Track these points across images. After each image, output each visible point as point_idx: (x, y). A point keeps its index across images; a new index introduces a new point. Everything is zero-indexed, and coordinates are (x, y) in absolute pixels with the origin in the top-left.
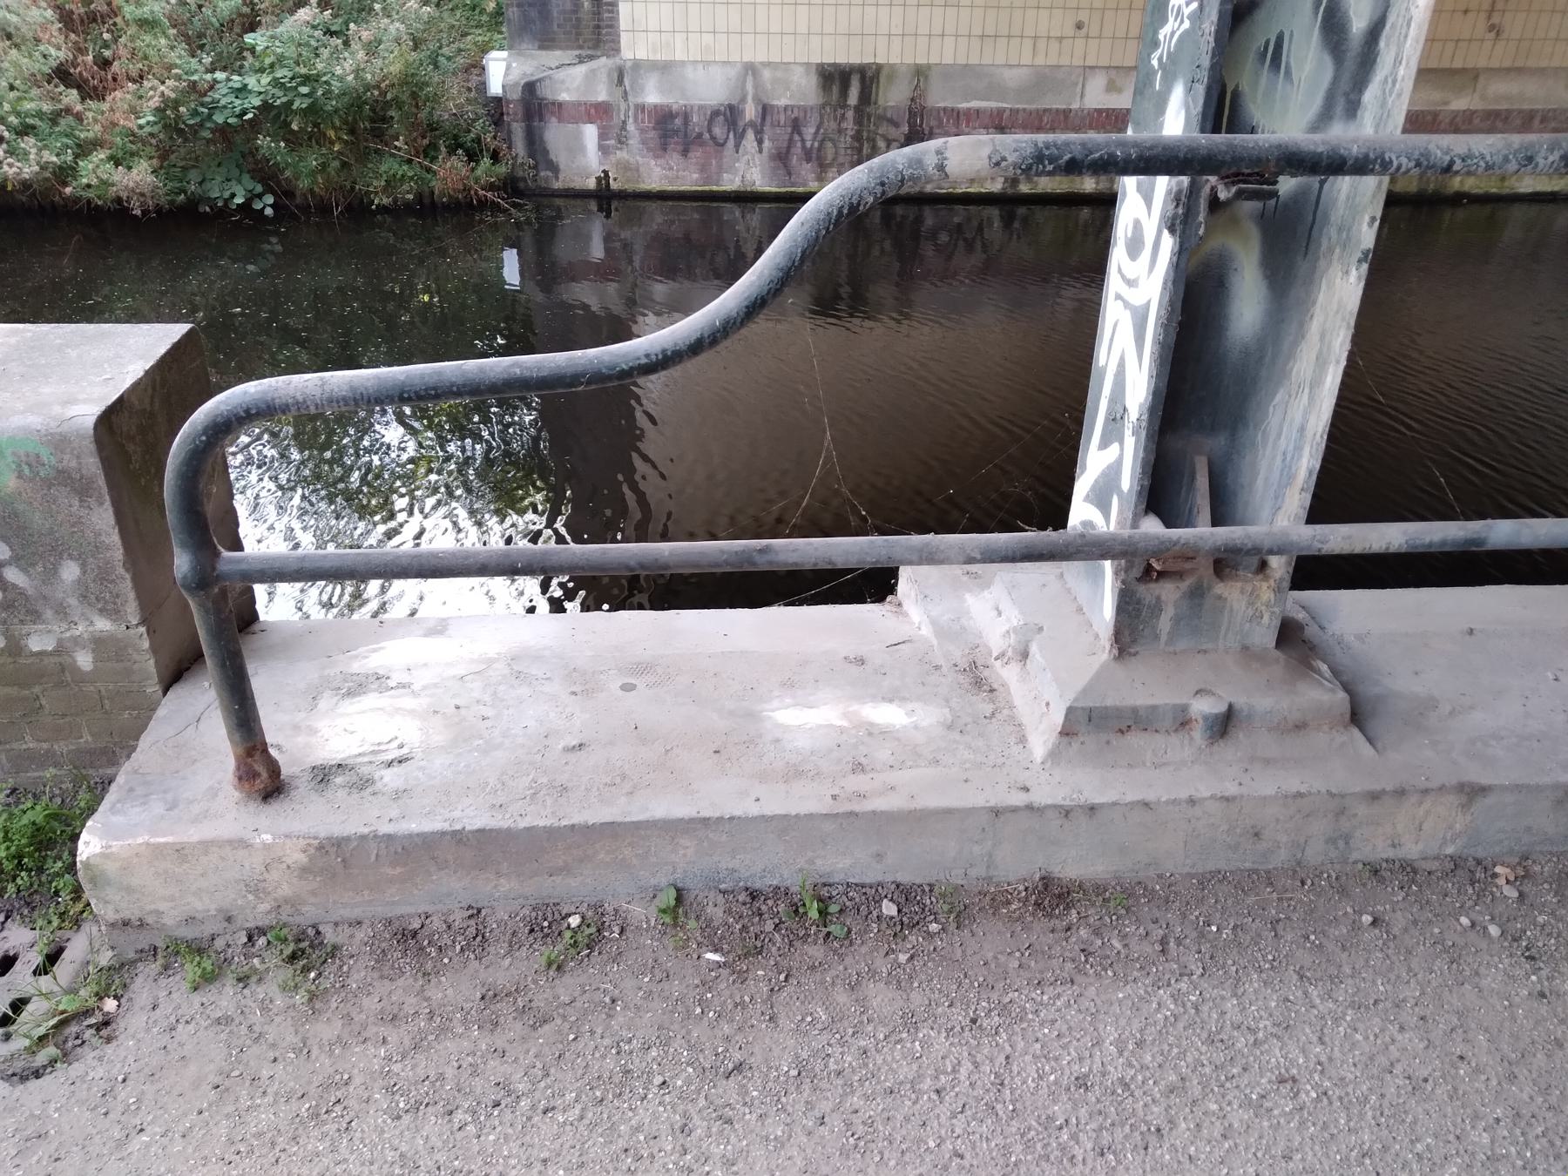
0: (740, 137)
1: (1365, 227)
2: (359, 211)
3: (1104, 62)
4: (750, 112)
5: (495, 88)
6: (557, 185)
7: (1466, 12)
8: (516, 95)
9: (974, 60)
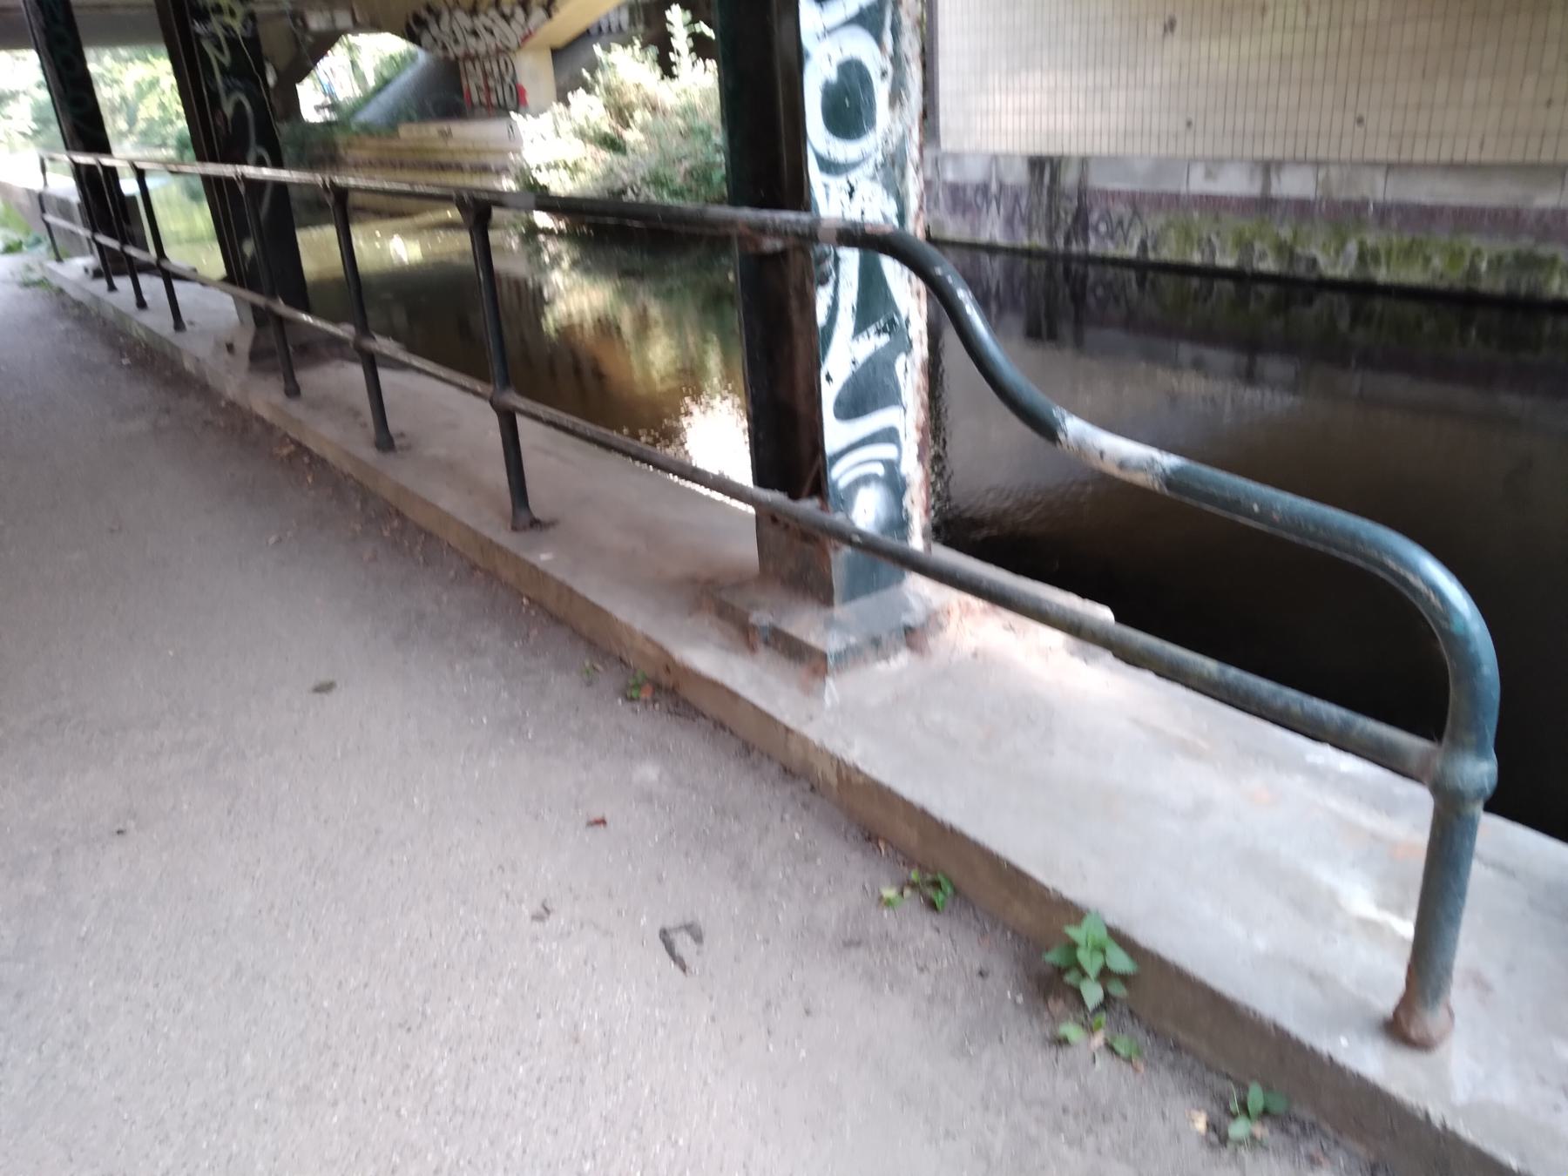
4: (994, 187)
9: (1121, 150)
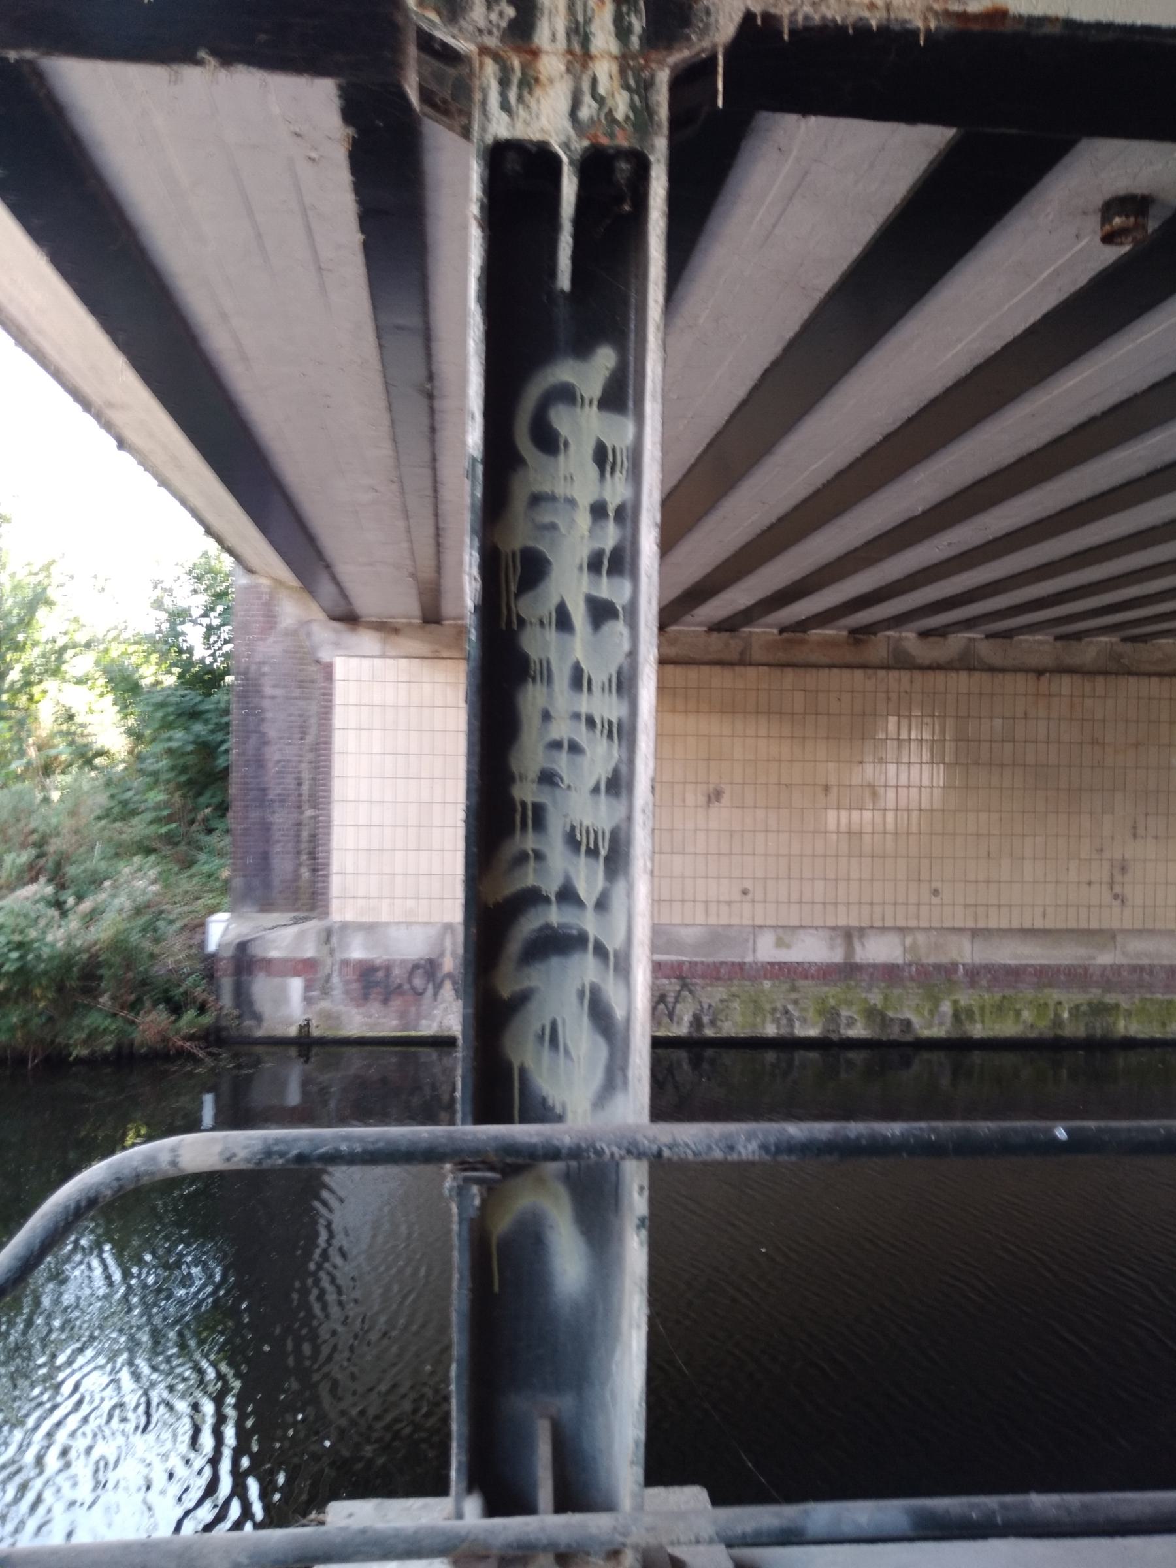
0: (438, 987)
1: (636, 1195)
2: (56, 1062)
3: (771, 922)
5: (212, 946)
6: (260, 1033)
7: (1090, 883)
8: (228, 953)
